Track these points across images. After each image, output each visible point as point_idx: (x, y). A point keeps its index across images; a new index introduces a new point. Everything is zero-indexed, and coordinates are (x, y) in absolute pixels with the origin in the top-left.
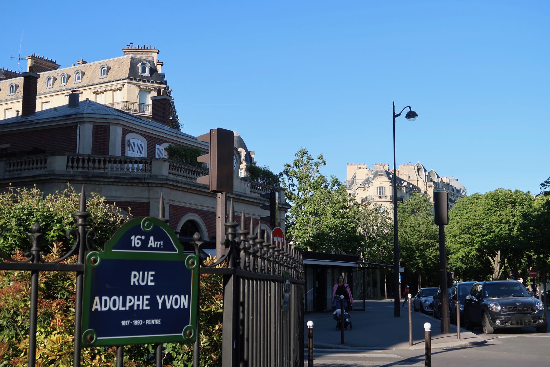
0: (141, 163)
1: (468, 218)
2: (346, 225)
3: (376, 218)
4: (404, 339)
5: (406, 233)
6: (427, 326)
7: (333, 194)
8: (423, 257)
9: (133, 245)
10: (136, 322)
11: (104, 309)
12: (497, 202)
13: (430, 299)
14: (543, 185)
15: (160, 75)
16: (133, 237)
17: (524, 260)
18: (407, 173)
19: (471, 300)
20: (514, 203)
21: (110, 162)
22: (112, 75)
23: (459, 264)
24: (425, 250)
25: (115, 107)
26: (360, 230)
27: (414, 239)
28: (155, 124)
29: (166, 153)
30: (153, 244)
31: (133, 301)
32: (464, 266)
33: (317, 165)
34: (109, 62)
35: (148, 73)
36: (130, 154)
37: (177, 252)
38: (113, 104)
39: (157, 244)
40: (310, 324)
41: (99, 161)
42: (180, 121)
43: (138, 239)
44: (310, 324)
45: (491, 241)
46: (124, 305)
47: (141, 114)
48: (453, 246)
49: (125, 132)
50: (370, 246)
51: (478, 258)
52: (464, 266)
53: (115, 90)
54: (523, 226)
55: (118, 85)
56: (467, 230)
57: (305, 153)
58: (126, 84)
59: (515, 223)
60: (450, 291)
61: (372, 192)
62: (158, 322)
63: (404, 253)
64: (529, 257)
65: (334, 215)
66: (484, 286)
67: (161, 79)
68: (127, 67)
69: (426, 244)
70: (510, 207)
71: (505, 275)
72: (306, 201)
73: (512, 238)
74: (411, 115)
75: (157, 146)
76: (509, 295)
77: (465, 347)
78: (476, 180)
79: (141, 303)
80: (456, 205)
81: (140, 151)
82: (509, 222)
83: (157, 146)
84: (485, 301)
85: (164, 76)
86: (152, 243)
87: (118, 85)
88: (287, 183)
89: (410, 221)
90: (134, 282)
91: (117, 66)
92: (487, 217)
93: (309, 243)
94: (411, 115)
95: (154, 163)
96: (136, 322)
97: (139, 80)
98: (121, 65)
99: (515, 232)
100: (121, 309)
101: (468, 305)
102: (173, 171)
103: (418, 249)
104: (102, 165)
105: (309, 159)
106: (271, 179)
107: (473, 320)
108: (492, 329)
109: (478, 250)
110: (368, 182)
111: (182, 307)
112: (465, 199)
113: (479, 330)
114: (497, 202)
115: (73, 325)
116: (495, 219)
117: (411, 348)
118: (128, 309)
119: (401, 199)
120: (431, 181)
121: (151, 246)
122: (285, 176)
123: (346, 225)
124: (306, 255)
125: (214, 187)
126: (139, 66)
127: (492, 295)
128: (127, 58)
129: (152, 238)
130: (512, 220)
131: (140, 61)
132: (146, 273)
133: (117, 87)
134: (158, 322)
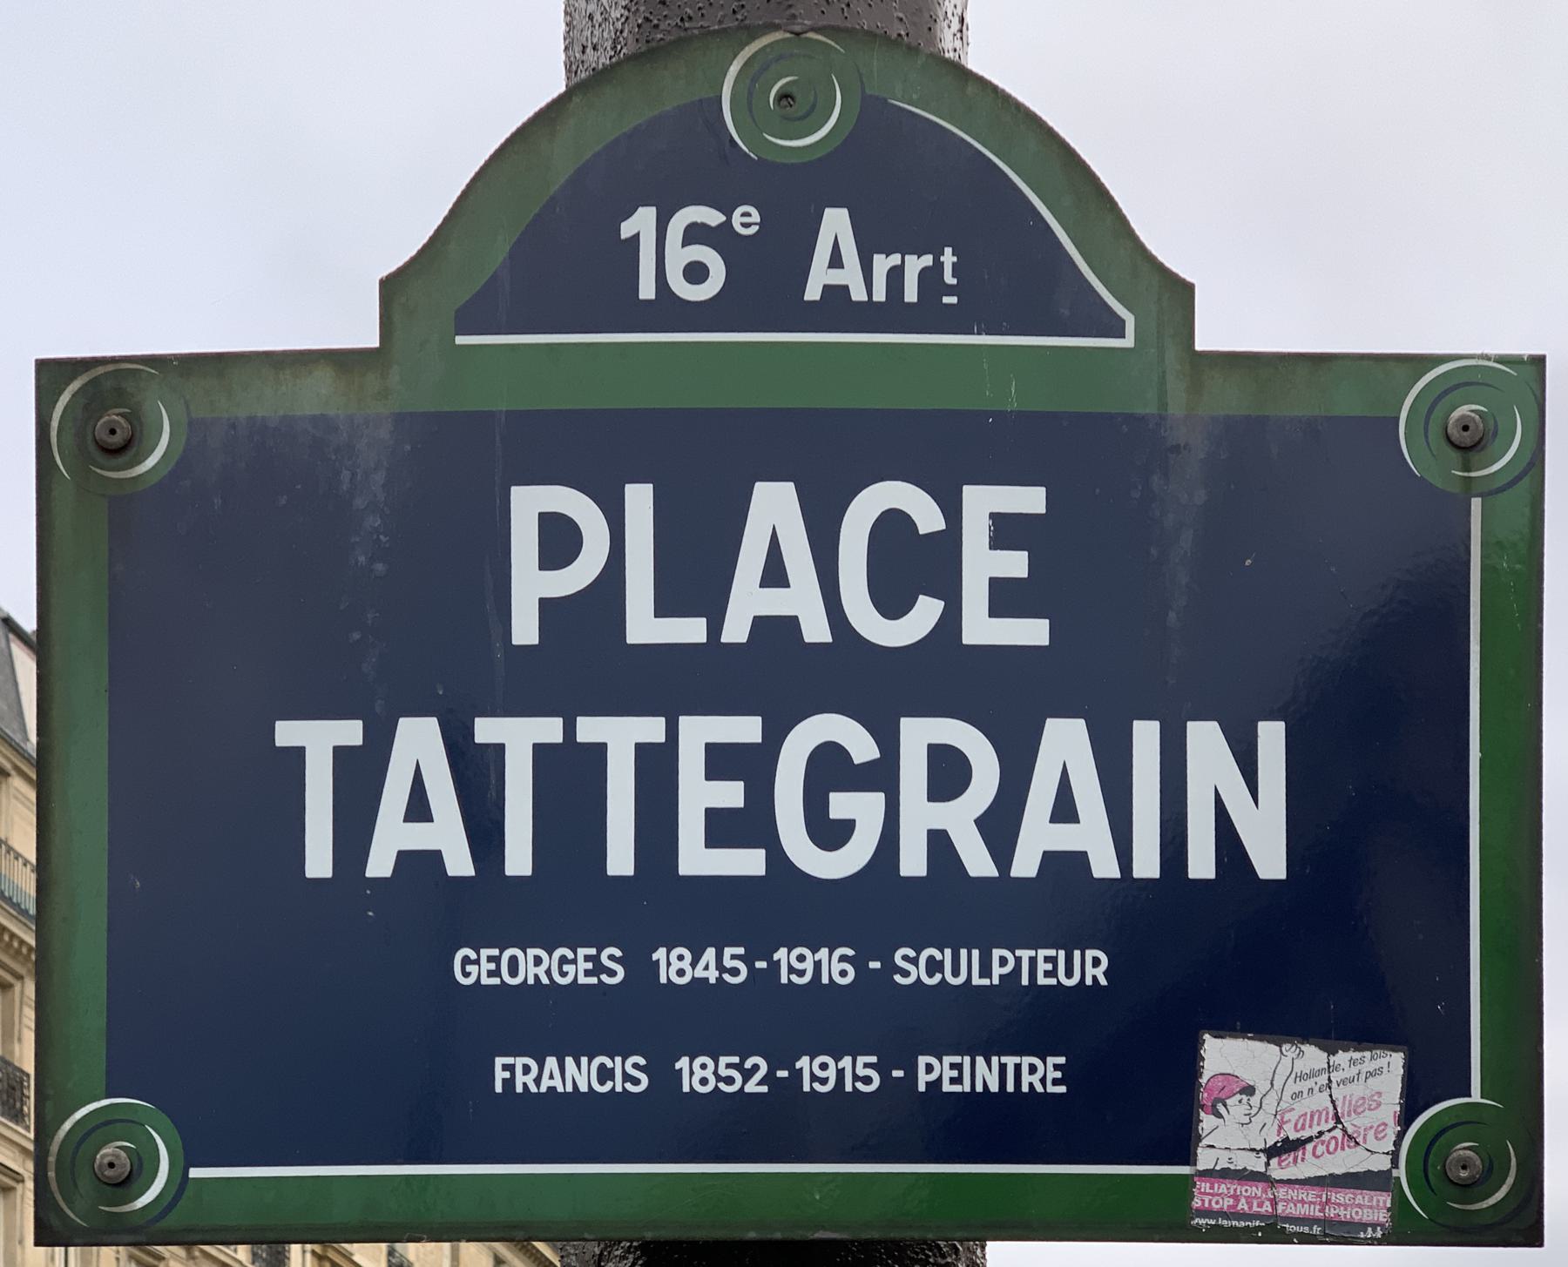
9: (647, 290)
11: (1010, 1061)
16: (641, 223)
30: (850, 276)
37: (1128, 342)
39: (896, 275)
43: (694, 234)
86: (836, 254)
90: (939, 842)
100: (976, 981)
111: (584, 1060)
118: (996, 981)
121: (835, 294)
129: (836, 224)
132: (1077, 953)
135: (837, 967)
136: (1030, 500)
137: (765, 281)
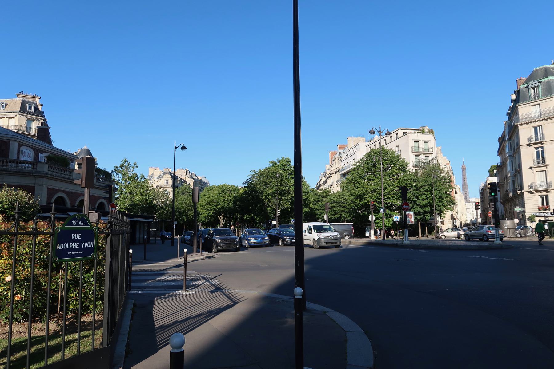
0: (30, 164)
1: (209, 198)
2: (147, 200)
3: (163, 196)
4: (175, 256)
5: (179, 204)
6: (185, 250)
7: (142, 184)
8: (187, 216)
10: (73, 253)
12: (223, 190)
13: (189, 237)
14: (244, 183)
15: (41, 112)
17: (234, 217)
18: (180, 174)
19: (208, 237)
20: (231, 191)
21: (10, 162)
22: (8, 109)
23: (204, 219)
24: (188, 212)
25: (10, 128)
26: (155, 202)
27: (183, 207)
28: (39, 141)
29: (46, 159)
31: (72, 245)
32: (207, 220)
33: (133, 168)
34: (7, 101)
35: (33, 110)
36: (23, 158)
38: (8, 126)
40: (131, 251)
41: (3, 162)
42: (52, 138)
44: (131, 251)
45: (220, 209)
46: (69, 246)
47: (27, 133)
48: (202, 211)
49: (20, 145)
50: (160, 210)
51: (213, 217)
52: (207, 220)
53: (10, 118)
54: (235, 202)
55: (12, 115)
56: (208, 203)
57: (126, 161)
58: (18, 115)
59: (231, 201)
60: (198, 233)
61: (162, 182)
62: (82, 252)
63: (177, 214)
64: (237, 216)
65: (141, 194)
66: (214, 231)
67: (41, 114)
68: (19, 105)
69: (188, 210)
70: (229, 192)
71: (225, 226)
72: (126, 186)
73: (229, 207)
74: (184, 148)
75: (40, 155)
76: (224, 235)
77: (202, 259)
78: (215, 179)
79: (76, 245)
80: (204, 190)
81: (29, 156)
82: (226, 201)
83: (40, 155)
84: (214, 238)
85: (43, 112)
86: (80, 223)
87: (12, 115)
88: (116, 176)
89: (181, 198)
91: (12, 104)
92: (218, 197)
93: (127, 209)
94: (184, 148)
95: (38, 165)
96: (73, 253)
97: (27, 114)
98: (16, 103)
99: (230, 205)
101: (206, 240)
102: (51, 169)
103: (184, 212)
104: (5, 164)
105: (128, 164)
106: (107, 175)
107: (208, 247)
108: (216, 251)
109: (213, 213)
110: (160, 177)
112: (208, 188)
113: (210, 251)
114: (223, 190)
115: (12, 255)
116: (222, 198)
117: (178, 260)
119: (177, 187)
120: (192, 178)
122: (114, 172)
123: (147, 200)
124: (123, 214)
125: (84, 185)
126: (27, 105)
127: (217, 235)
128: (19, 100)
130: (229, 199)
131: (28, 102)
133: (11, 116)
134: (82, 252)
137: (78, 223)
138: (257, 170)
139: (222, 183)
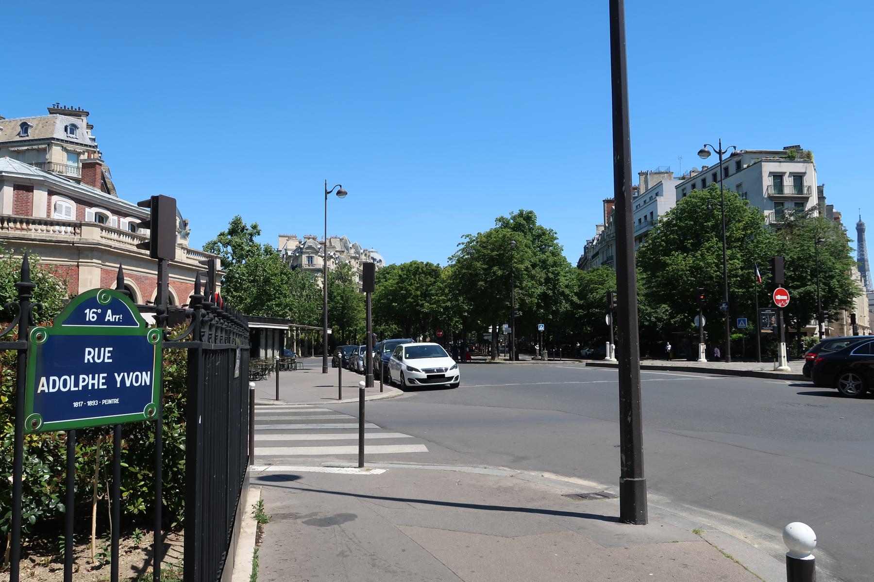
10: (90, 403)
14: (450, 259)
16: (87, 311)
30: (110, 318)
31: (87, 381)
43: (94, 313)
46: (76, 384)
62: (116, 401)
79: (98, 382)
81: (68, 213)
86: (109, 316)
96: (90, 403)
100: (73, 389)
129: (109, 312)
134: (116, 401)
135: (92, 315)
136: (105, 375)
137: (101, 319)
138: (475, 234)
139: (408, 261)
